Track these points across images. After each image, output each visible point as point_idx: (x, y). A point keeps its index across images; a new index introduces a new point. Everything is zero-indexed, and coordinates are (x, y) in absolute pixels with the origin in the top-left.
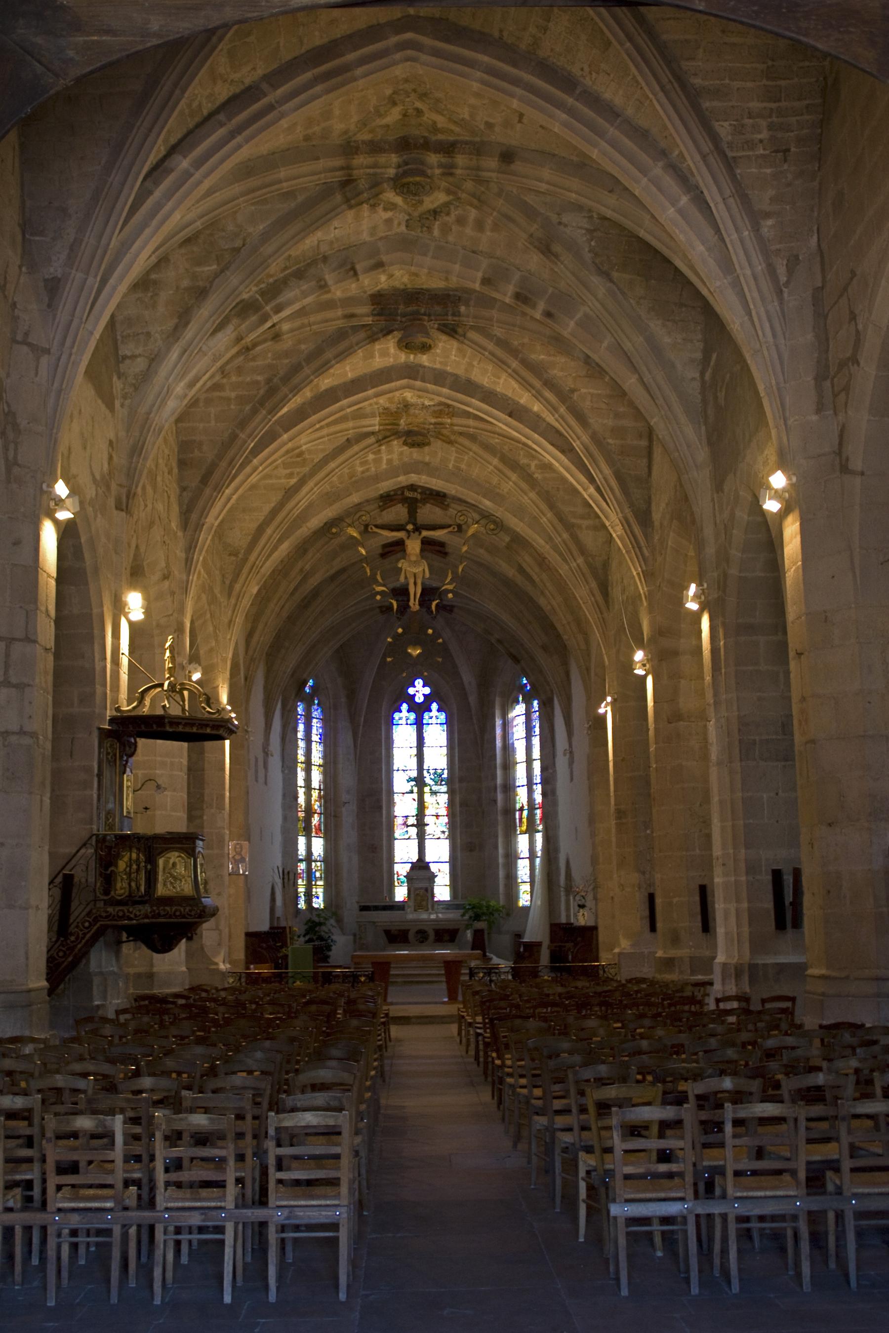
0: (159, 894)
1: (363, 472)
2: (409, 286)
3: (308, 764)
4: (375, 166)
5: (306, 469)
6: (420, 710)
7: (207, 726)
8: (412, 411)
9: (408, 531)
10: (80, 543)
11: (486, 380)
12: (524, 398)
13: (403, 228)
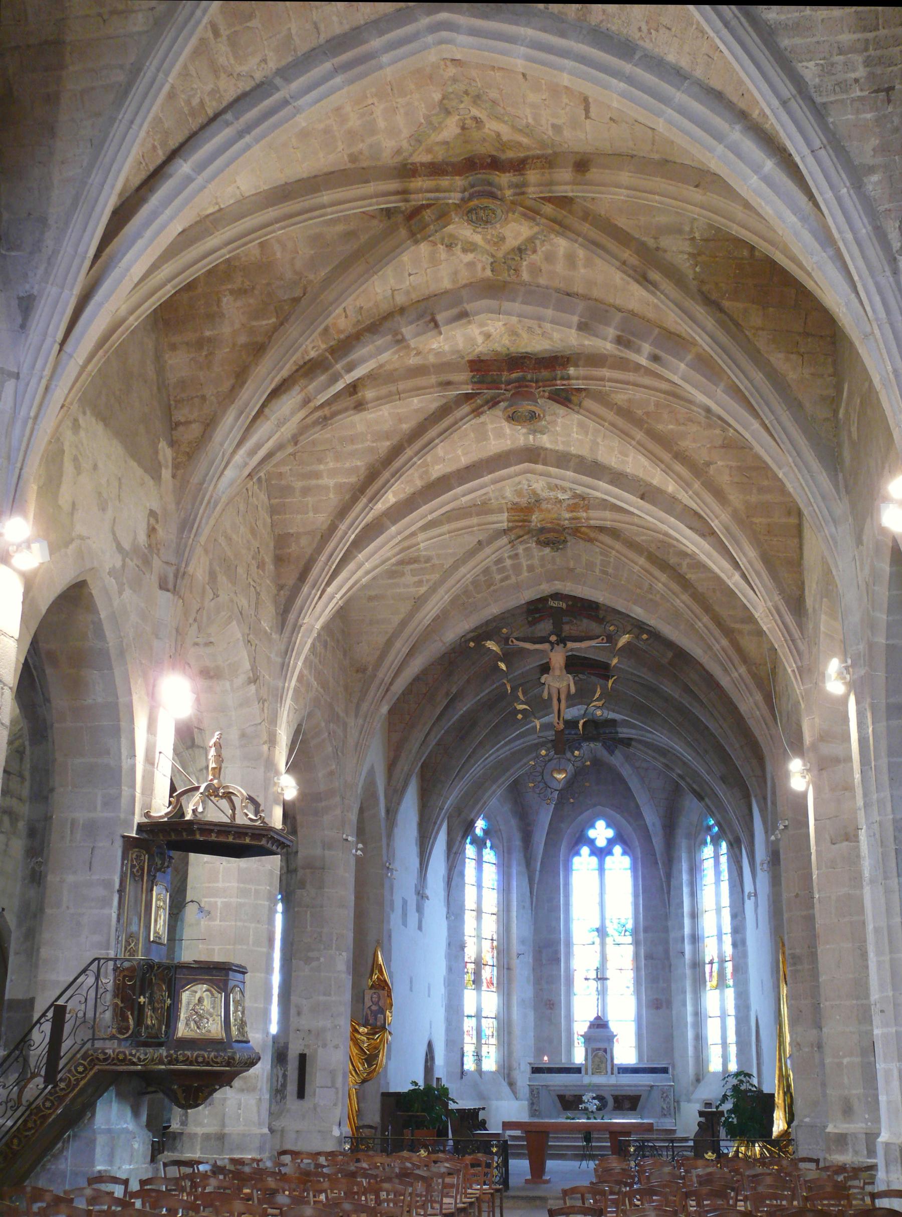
0: (180, 1035)
1: (502, 580)
2: (512, 349)
3: (479, 912)
4: (437, 190)
5: (436, 577)
6: (601, 853)
7: (246, 834)
8: (544, 506)
9: (551, 643)
10: (100, 619)
11: (614, 459)
12: (657, 477)
13: (488, 273)
